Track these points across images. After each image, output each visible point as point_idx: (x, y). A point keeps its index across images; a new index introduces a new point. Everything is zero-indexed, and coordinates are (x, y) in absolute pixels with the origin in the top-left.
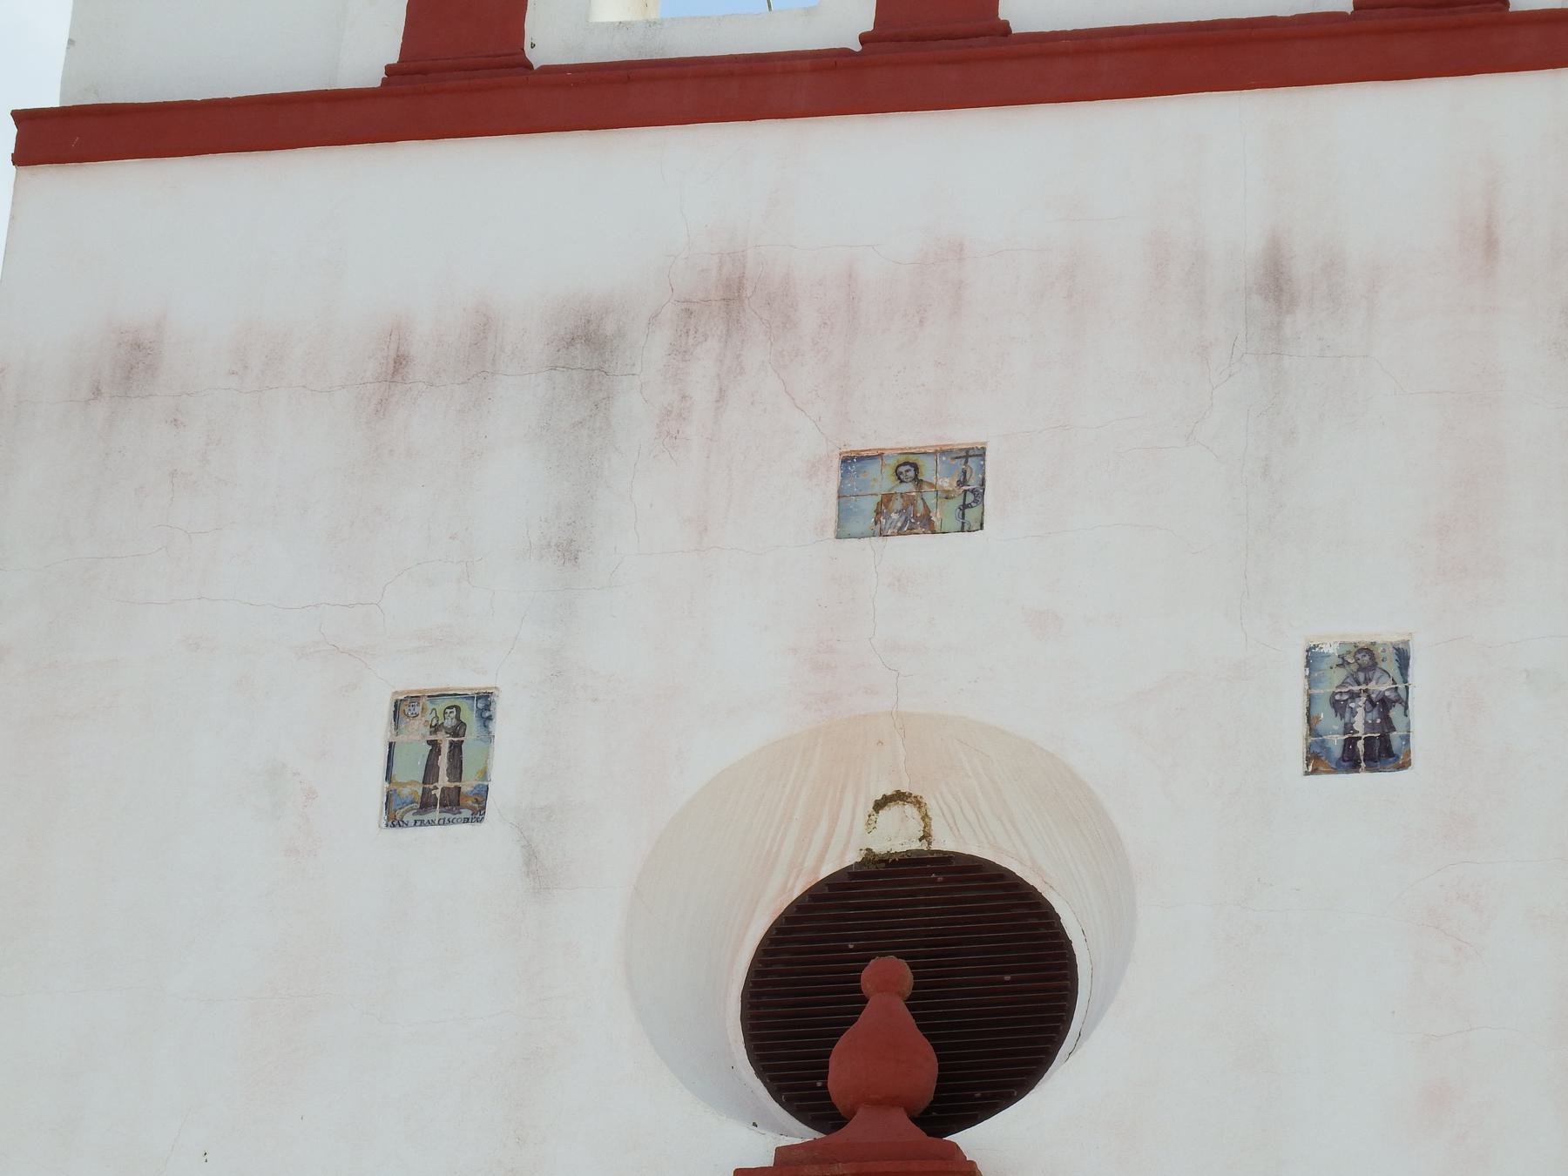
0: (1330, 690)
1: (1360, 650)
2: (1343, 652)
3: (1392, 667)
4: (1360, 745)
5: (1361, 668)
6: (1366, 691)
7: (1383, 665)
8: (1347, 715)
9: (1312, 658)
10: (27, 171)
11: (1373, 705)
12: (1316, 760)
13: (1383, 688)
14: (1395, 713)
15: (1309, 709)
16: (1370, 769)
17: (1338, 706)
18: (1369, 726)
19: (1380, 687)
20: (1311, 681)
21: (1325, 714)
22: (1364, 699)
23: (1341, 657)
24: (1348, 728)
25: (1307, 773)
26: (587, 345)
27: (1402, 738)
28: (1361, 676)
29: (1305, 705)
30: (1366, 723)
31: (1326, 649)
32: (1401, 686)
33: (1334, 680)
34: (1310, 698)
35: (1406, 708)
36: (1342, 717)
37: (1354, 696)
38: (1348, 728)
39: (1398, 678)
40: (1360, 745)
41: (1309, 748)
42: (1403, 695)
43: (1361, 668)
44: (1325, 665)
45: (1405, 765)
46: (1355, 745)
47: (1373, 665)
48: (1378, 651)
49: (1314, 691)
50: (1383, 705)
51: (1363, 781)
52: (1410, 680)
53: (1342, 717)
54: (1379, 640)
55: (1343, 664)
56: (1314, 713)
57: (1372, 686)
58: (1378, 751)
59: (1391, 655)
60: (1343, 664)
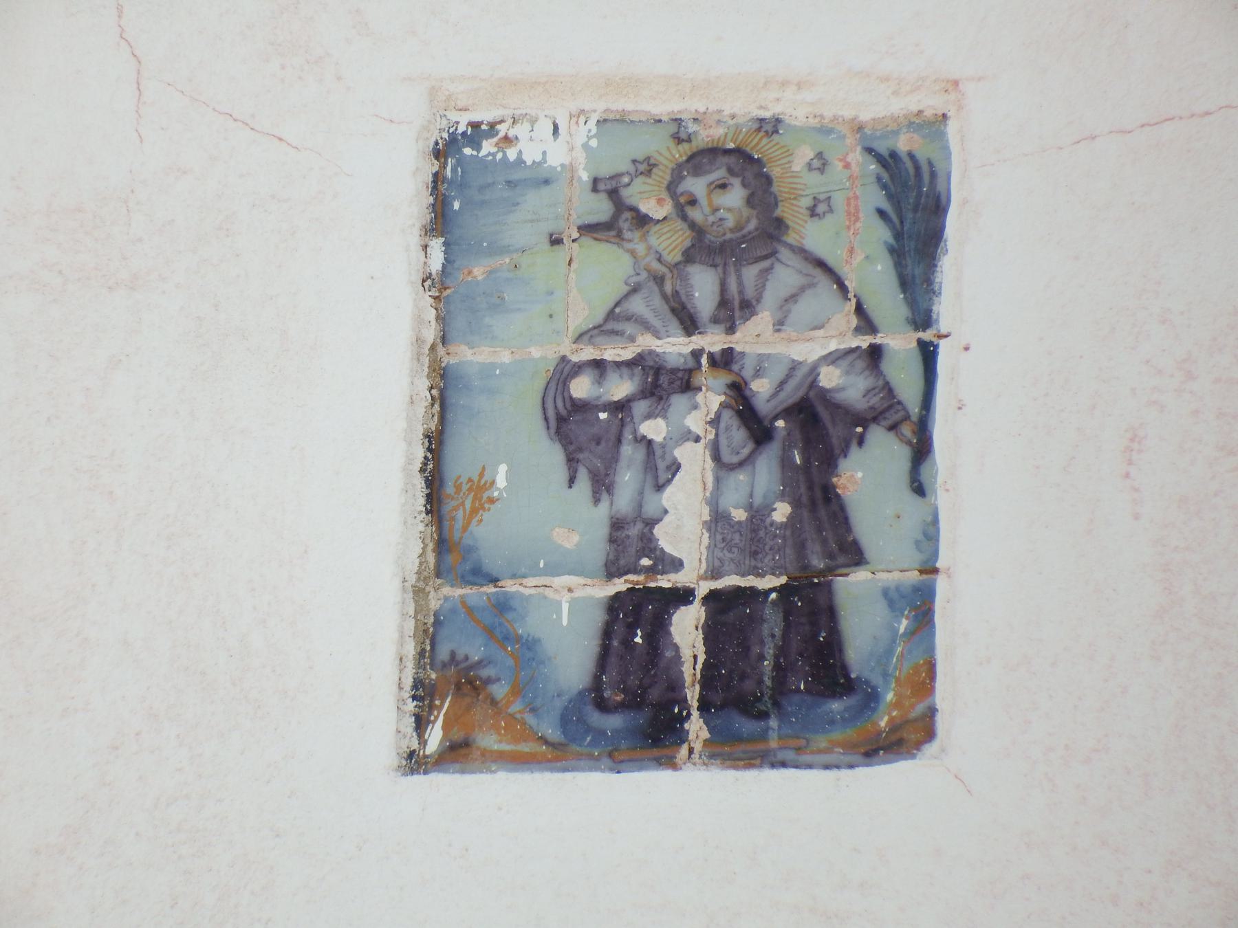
0: (544, 354)
1: (702, 158)
2: (616, 162)
3: (858, 245)
4: (687, 629)
5: (705, 247)
6: (724, 360)
7: (816, 236)
8: (628, 478)
9: (462, 183)
10: (880, 327)
11: (760, 433)
12: (463, 697)
13: (807, 351)
14: (868, 476)
15: (436, 443)
16: (734, 749)
17: (583, 433)
18: (737, 537)
19: (796, 342)
20: (451, 299)
21: (518, 470)
22: (711, 398)
23: (609, 188)
24: (630, 542)
25: (414, 763)
26: (875, 353)
27: (893, 599)
28: (703, 288)
29: (420, 419)
30: (718, 520)
31: (534, 146)
32: (899, 343)
33: (561, 303)
34: (445, 388)
35: (922, 450)
36: (602, 485)
37: (663, 383)
38: (630, 542)
39: (887, 303)
40: (687, 629)
41: (430, 635)
42: (908, 388)
43: (705, 247)
44: (524, 224)
45: (909, 736)
46: (658, 629)
47: (768, 233)
48: (793, 166)
49: (465, 355)
50: (811, 432)
51: (695, 803)
52: (946, 310)
53: (602, 485)
54: (796, 109)
55: (617, 220)
56: (459, 467)
57: (754, 338)
58: (774, 660)
59: (856, 184)
60: (617, 220)
